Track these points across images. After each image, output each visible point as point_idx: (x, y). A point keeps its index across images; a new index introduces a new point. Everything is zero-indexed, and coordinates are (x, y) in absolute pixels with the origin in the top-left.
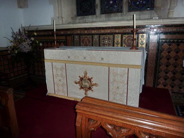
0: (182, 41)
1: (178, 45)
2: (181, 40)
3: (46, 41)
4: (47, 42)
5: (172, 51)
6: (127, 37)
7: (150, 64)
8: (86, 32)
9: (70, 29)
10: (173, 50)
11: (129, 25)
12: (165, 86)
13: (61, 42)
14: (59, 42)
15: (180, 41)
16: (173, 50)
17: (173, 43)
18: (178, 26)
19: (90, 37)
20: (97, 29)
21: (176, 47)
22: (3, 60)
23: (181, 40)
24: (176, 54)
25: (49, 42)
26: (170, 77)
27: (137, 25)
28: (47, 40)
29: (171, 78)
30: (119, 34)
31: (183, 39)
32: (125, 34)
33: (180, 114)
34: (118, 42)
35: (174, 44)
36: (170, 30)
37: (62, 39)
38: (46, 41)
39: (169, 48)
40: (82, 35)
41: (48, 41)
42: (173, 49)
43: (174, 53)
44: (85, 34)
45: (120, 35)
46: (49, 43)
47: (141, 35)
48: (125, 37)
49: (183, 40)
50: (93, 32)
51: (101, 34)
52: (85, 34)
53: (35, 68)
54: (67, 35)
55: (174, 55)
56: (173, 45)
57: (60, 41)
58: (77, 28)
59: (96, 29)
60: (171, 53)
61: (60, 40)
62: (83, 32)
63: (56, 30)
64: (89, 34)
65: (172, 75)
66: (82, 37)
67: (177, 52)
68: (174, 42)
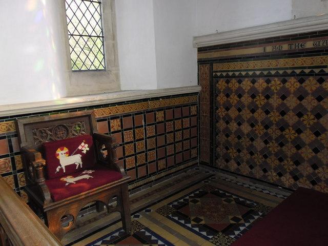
0: (322, 71)
1: (301, 81)
2: (267, 72)
3: (224, 74)
4: (227, 76)
7: (202, 117)
12: (314, 183)
17: (311, 75)
22: (145, 126)
23: (267, 72)
24: (298, 102)
28: (255, 70)
31: (326, 67)
33: (241, 218)
38: (224, 74)
39: (283, 88)
41: (231, 74)
45: (208, 66)
46: (276, 79)
49: (324, 69)
56: (290, 82)
57: (227, 74)
67: (301, 98)
68: (293, 74)
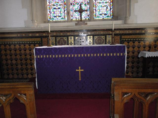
2: (130, 39)
5: (130, 47)
6: (98, 38)
8: (62, 34)
9: (46, 31)
10: (131, 46)
11: (41, 31)
13: (36, 43)
14: (133, 41)
15: (134, 40)
16: (131, 46)
18: (133, 30)
19: (96, 38)
20: (72, 31)
21: (133, 44)
23: (130, 39)
25: (17, 44)
26: (130, 66)
27: (51, 30)
29: (131, 67)
30: (91, 35)
32: (96, 35)
34: (71, 42)
35: (131, 42)
36: (97, 33)
37: (15, 41)
40: (58, 36)
42: (131, 45)
43: (132, 48)
44: (60, 36)
47: (70, 37)
48: (103, 37)
50: (68, 34)
51: (94, 35)
52: (60, 36)
53: (4, 71)
54: (43, 37)
55: (132, 50)
58: (53, 31)
59: (103, 30)
60: (130, 48)
61: (35, 41)
62: (58, 34)
63: (50, 31)
64: (64, 36)
65: (132, 64)
66: (58, 39)
